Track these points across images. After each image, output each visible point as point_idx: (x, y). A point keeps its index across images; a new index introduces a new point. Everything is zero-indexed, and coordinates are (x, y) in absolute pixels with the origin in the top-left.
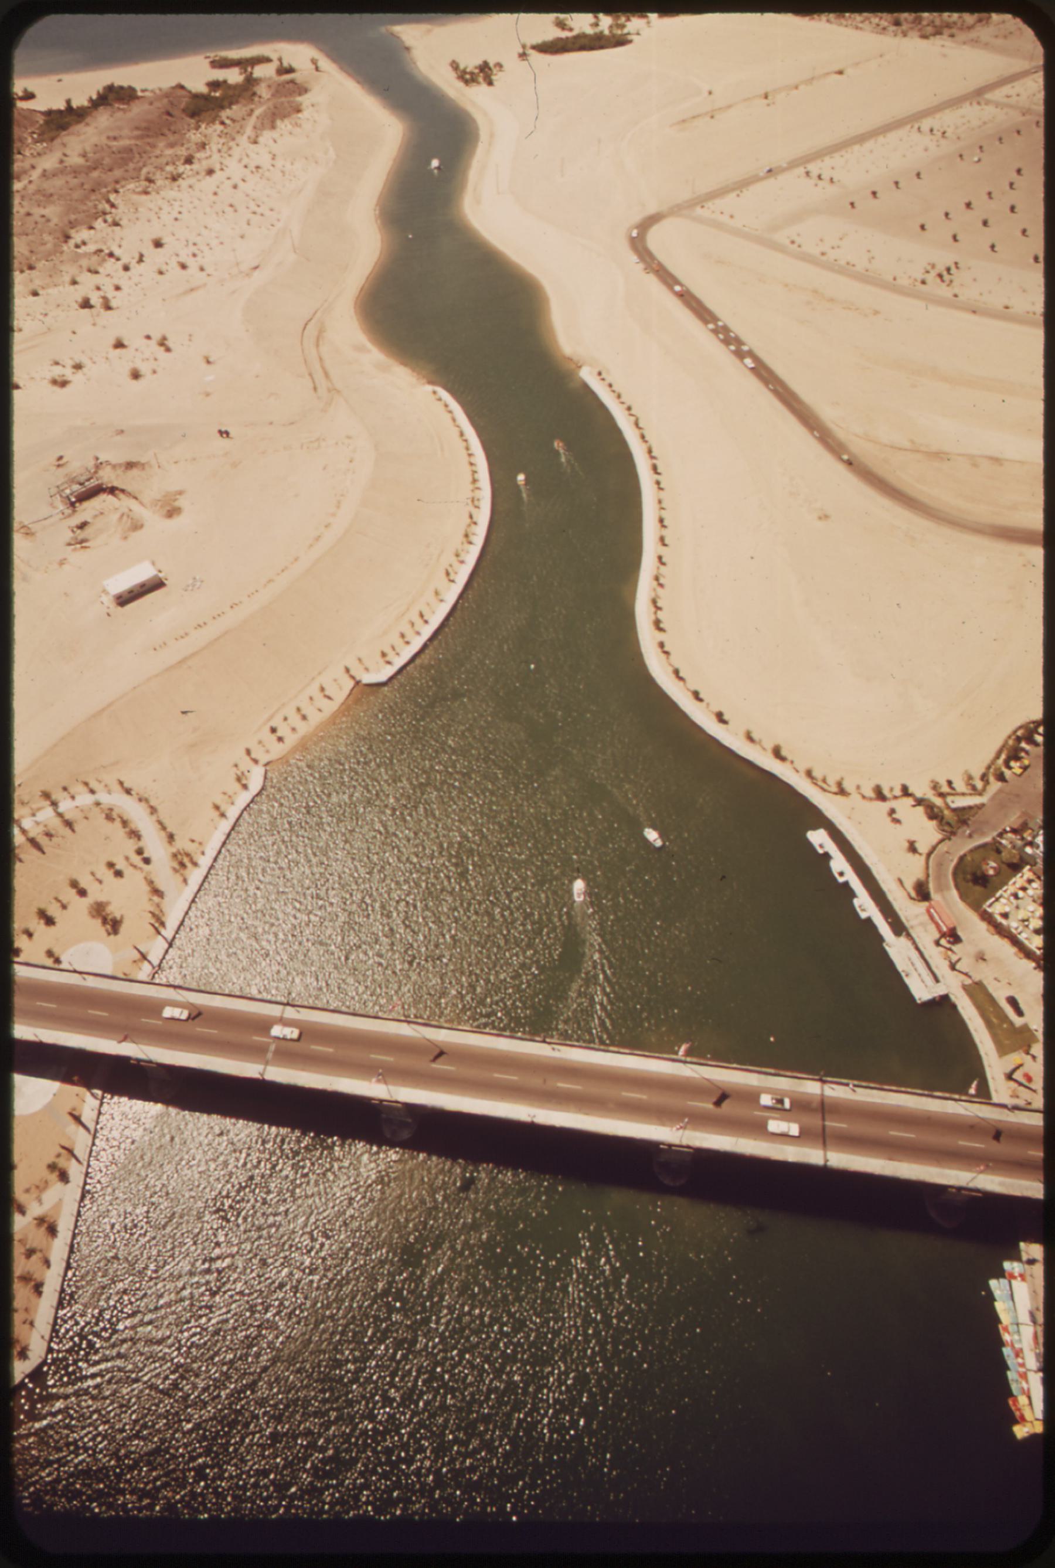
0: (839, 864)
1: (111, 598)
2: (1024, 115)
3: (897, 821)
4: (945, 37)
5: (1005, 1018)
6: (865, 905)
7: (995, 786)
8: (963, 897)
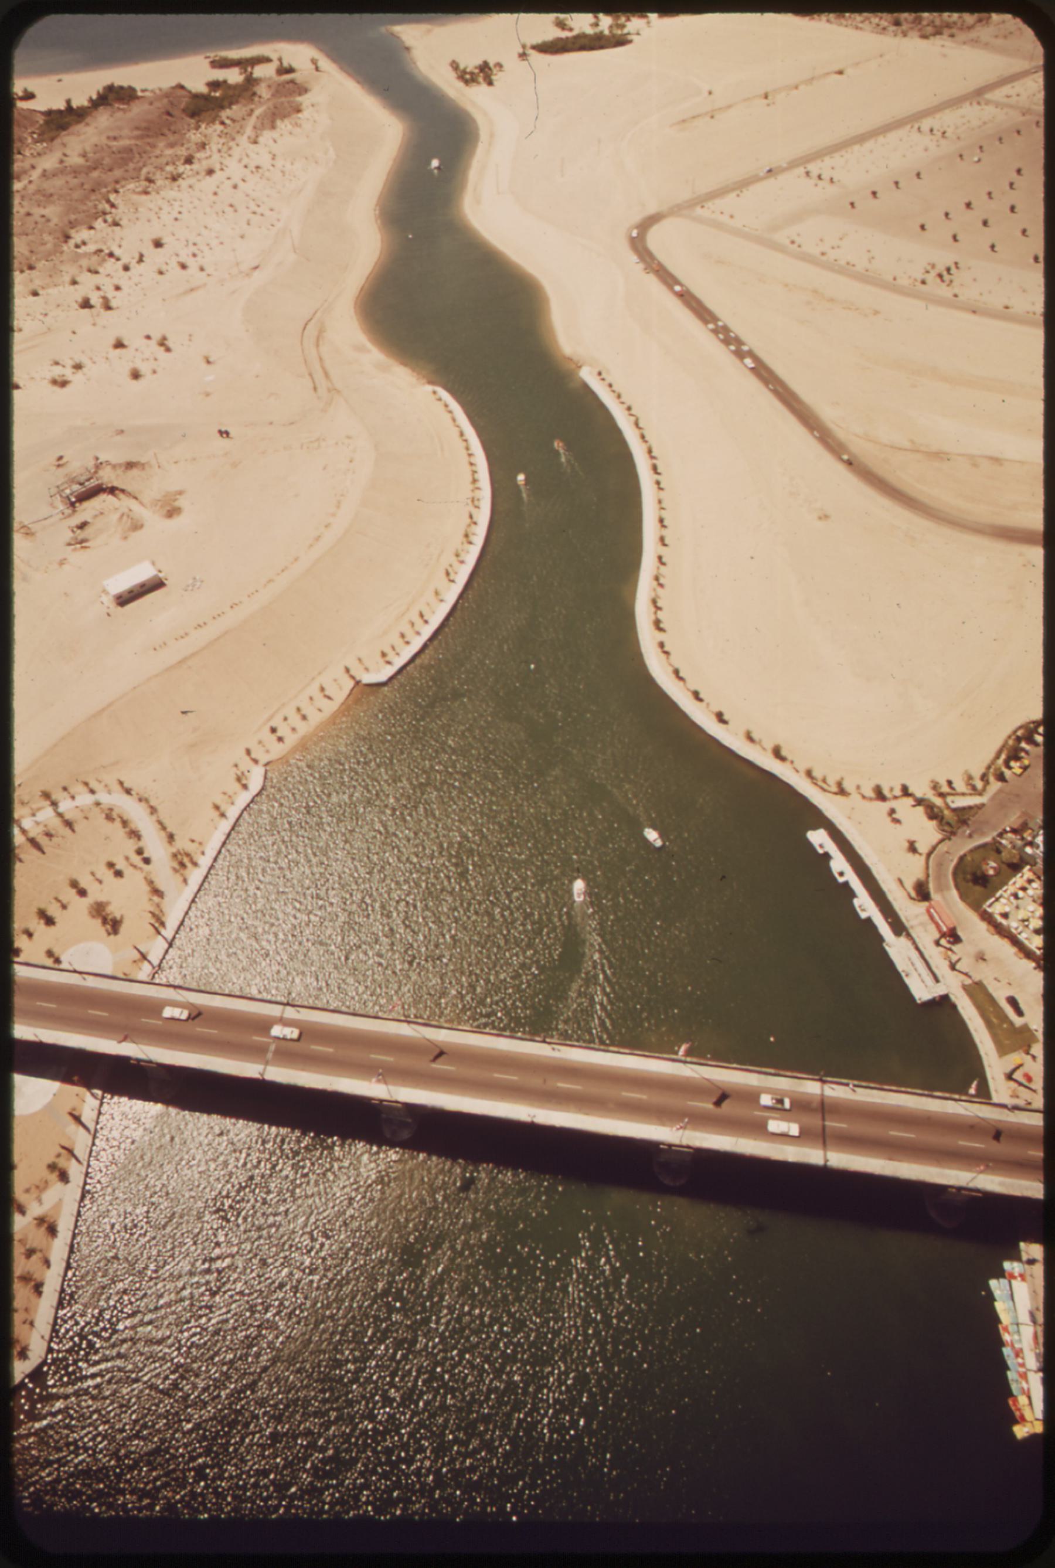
0: (839, 864)
1: (111, 598)
2: (1024, 115)
3: (897, 821)
4: (945, 37)
5: (1005, 1018)
6: (865, 905)
7: (995, 786)
8: (963, 897)
